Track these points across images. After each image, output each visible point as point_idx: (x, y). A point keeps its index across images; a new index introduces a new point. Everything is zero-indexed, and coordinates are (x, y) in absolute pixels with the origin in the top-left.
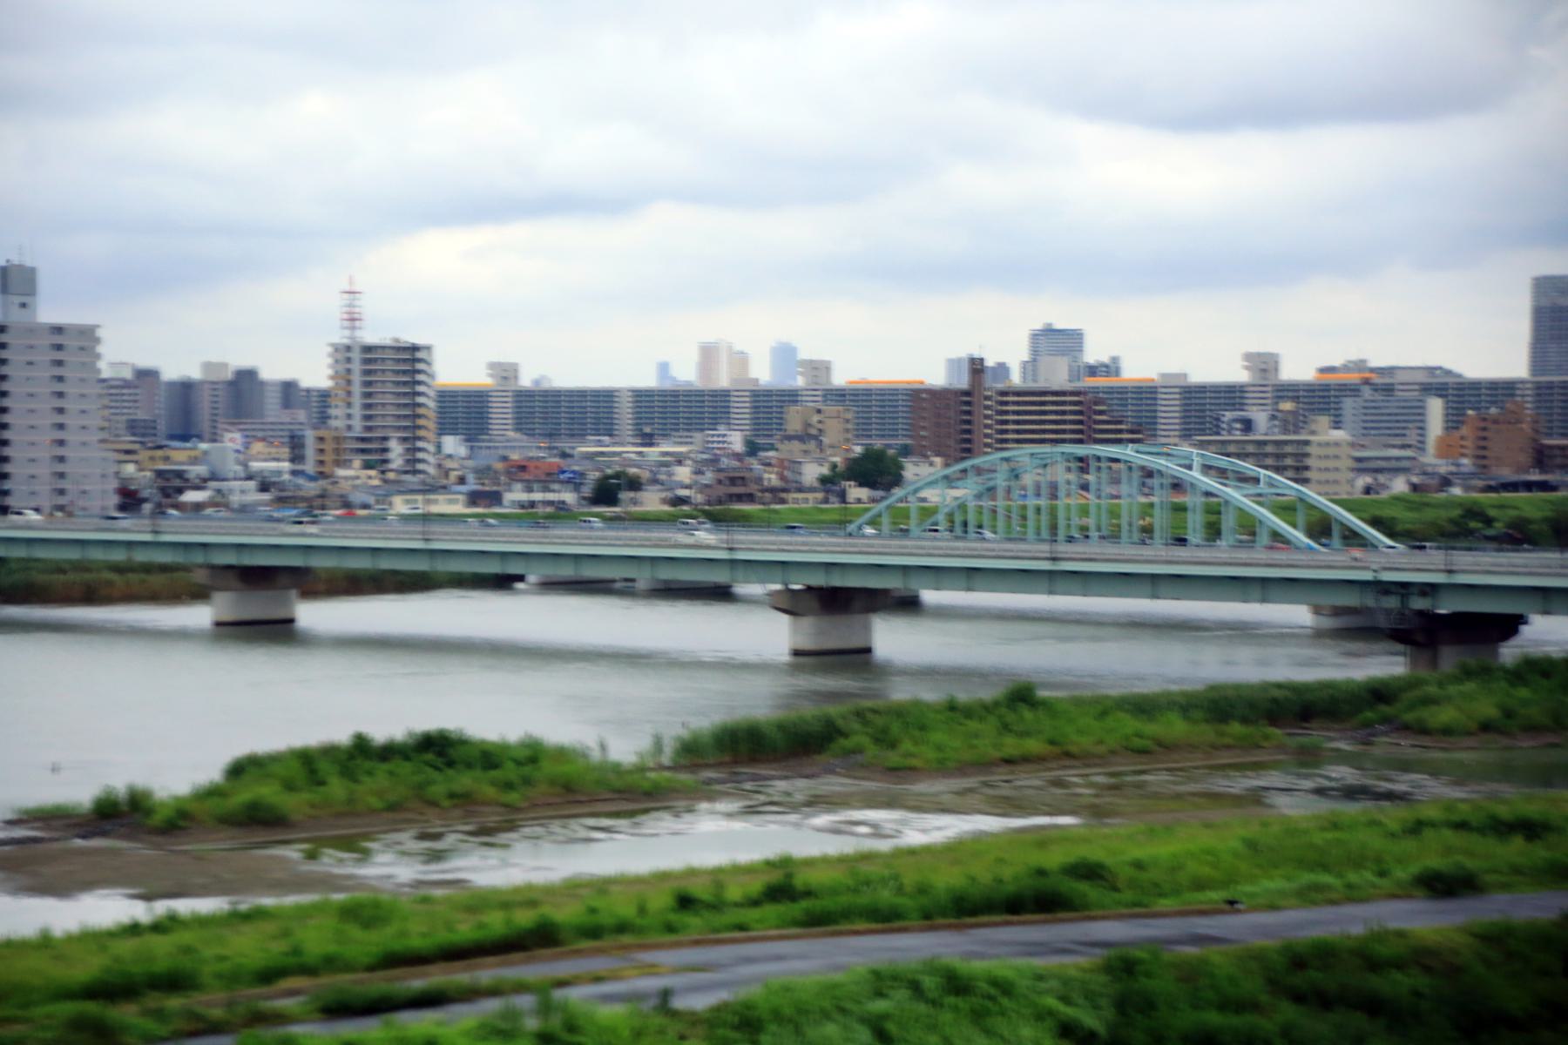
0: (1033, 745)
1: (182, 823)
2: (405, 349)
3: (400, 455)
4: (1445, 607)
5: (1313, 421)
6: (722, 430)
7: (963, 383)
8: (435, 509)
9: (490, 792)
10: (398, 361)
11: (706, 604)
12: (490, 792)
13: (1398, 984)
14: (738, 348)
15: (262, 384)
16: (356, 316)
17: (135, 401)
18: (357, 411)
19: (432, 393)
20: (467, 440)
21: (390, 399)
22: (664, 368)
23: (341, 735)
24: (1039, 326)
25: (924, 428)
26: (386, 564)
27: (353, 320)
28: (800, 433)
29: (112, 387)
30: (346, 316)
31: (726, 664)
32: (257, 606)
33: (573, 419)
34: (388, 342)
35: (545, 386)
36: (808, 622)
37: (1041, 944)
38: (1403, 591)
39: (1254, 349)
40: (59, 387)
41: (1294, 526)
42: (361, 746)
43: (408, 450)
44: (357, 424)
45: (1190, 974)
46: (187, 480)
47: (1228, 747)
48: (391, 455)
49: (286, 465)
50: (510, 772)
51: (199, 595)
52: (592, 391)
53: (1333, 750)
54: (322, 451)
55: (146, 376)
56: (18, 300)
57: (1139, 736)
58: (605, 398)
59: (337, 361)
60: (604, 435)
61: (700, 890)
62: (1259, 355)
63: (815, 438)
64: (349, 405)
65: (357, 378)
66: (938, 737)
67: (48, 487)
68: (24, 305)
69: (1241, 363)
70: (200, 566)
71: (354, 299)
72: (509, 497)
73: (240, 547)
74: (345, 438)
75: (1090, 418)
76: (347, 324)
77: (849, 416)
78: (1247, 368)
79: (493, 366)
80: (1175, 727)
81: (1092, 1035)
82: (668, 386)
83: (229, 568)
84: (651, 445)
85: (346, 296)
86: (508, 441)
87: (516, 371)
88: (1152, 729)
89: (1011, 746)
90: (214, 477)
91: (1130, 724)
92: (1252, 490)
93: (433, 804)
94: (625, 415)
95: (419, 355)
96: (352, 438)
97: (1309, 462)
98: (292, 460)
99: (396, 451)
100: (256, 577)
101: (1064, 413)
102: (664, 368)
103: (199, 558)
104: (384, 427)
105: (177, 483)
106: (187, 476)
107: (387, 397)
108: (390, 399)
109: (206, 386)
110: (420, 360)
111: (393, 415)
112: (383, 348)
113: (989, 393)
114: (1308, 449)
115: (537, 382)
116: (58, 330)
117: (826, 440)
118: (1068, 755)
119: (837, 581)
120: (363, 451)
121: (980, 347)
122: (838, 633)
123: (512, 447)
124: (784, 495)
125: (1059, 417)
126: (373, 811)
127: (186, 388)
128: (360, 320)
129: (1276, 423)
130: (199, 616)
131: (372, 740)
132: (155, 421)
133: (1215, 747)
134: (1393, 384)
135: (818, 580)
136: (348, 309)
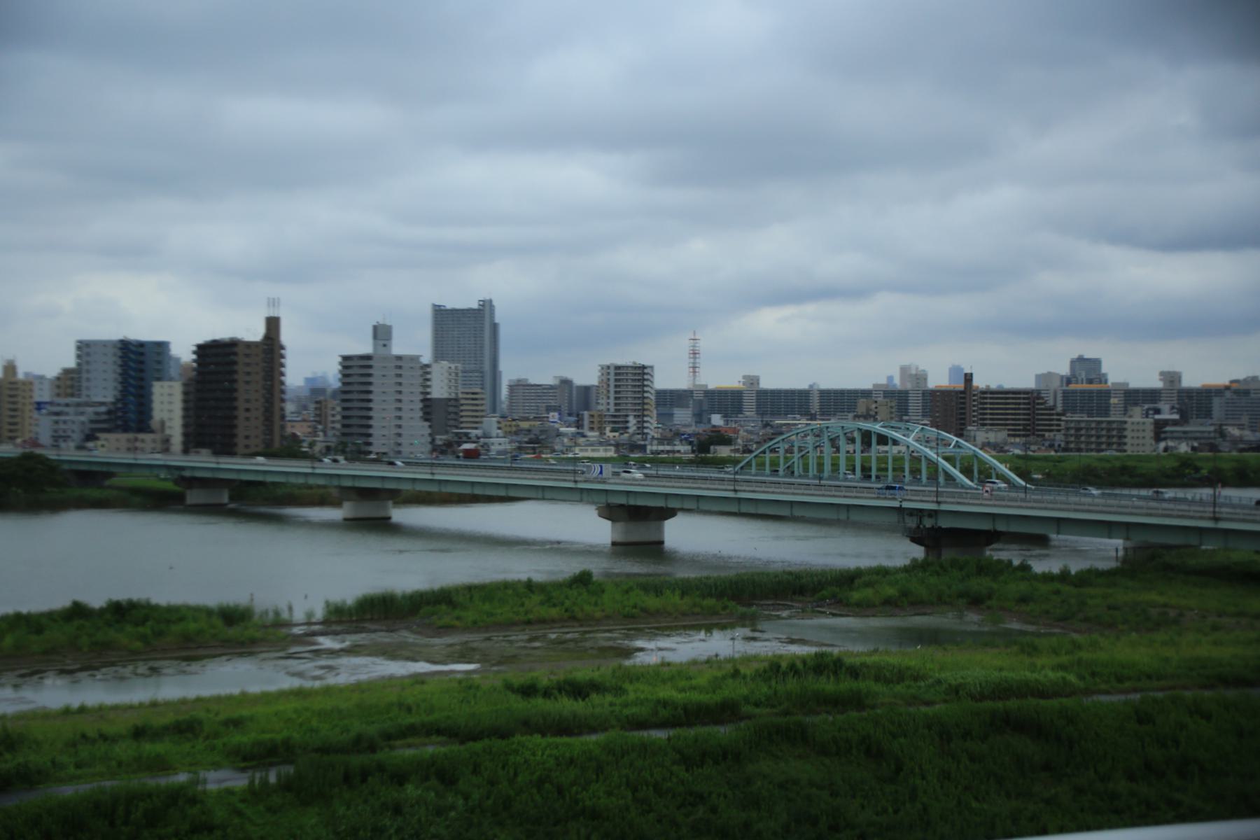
4: (945, 523)
5: (1132, 410)
7: (960, 386)
10: (635, 374)
11: (333, 520)
16: (697, 352)
17: (555, 396)
18: (612, 401)
19: (653, 392)
20: (724, 417)
21: (630, 395)
23: (60, 602)
24: (1075, 356)
25: (938, 412)
27: (695, 354)
28: (865, 414)
30: (691, 352)
31: (590, 552)
32: (368, 510)
33: (788, 405)
34: (631, 364)
36: (620, 526)
38: (920, 514)
39: (1166, 369)
40: (399, 388)
41: (955, 467)
42: (78, 611)
43: (639, 422)
44: (612, 408)
46: (470, 438)
51: (336, 504)
52: (848, 391)
54: (592, 422)
55: (566, 383)
56: (382, 342)
59: (603, 374)
60: (798, 414)
62: (1169, 373)
63: (874, 417)
64: (608, 398)
65: (612, 383)
67: (392, 442)
68: (385, 345)
69: (1157, 377)
71: (696, 343)
73: (354, 477)
74: (605, 415)
76: (692, 356)
77: (893, 404)
78: (1161, 380)
85: (692, 341)
86: (747, 417)
87: (758, 380)
94: (815, 406)
95: (646, 371)
96: (610, 415)
97: (1126, 433)
98: (578, 427)
99: (632, 421)
101: (1019, 404)
103: (335, 482)
104: (627, 409)
106: (470, 435)
108: (630, 395)
109: (594, 388)
110: (647, 374)
111: (631, 403)
112: (627, 367)
113: (976, 393)
114: (1126, 426)
116: (399, 358)
118: (573, 618)
119: (640, 502)
122: (641, 533)
123: (749, 421)
125: (1017, 406)
128: (698, 353)
129: (1175, 410)
132: (560, 407)
133: (684, 614)
134: (1249, 390)
135: (622, 500)
136: (691, 348)
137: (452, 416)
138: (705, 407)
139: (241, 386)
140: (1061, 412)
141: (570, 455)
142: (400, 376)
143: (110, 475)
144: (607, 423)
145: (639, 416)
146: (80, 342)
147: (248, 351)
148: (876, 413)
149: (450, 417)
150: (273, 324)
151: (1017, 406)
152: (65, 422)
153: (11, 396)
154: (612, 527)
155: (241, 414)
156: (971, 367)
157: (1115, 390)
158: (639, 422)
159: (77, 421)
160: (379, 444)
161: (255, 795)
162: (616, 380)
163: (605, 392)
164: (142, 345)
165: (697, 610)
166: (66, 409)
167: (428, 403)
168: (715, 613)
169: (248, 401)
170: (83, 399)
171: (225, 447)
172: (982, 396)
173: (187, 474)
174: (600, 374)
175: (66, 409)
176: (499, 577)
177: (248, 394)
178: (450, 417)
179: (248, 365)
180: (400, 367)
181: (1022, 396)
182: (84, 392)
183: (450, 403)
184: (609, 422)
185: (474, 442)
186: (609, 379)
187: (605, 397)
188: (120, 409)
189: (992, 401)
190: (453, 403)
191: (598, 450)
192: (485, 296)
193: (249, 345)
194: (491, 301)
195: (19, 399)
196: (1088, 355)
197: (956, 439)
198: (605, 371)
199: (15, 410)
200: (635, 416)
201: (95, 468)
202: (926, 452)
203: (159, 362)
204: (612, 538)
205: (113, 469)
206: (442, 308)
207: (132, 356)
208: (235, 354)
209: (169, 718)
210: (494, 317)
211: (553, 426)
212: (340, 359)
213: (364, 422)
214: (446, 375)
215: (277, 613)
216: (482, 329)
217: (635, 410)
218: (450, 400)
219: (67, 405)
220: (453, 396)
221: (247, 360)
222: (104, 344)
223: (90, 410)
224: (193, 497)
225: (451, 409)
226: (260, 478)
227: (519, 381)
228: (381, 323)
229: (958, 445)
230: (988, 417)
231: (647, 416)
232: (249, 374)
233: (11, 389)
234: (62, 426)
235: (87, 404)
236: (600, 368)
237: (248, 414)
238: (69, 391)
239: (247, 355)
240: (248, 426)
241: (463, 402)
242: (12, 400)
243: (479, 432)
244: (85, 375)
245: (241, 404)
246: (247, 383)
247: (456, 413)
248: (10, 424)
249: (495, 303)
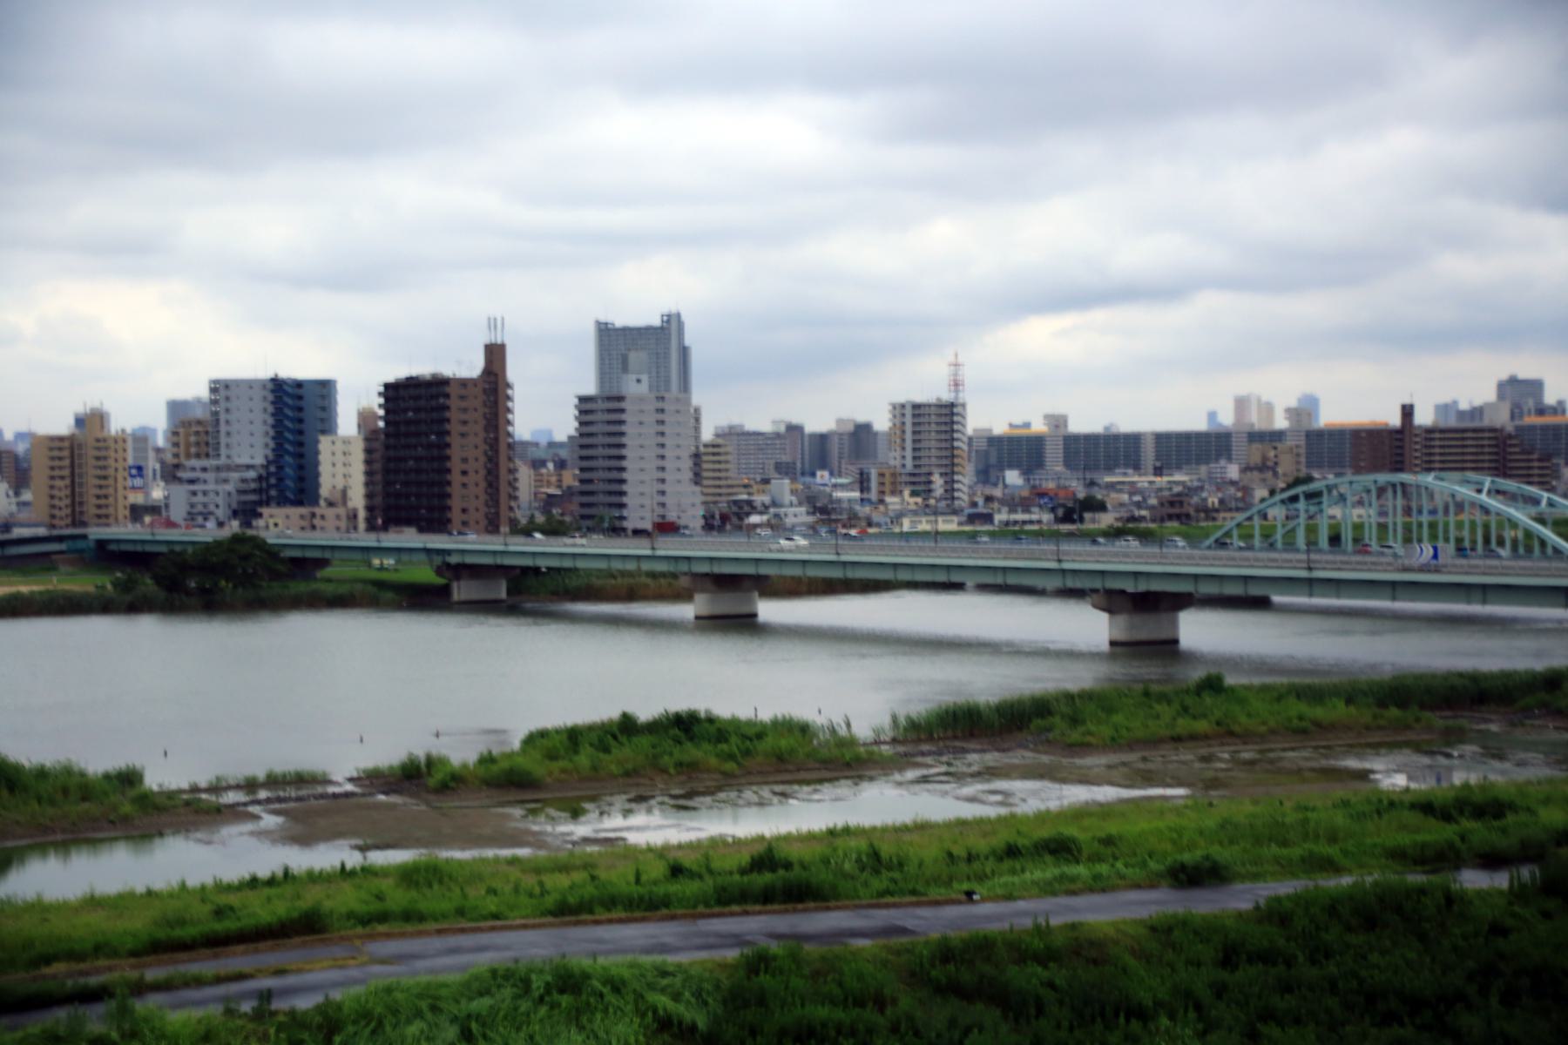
0: (1202, 726)
1: (452, 784)
2: (945, 406)
3: (941, 486)
6: (1223, 462)
7: (1395, 420)
8: (512, 548)
9: (713, 761)
12: (713, 761)
13: (1028, 977)
14: (1265, 398)
15: (876, 434)
18: (909, 453)
22: (1212, 416)
24: (1504, 376)
26: (812, 572)
29: (769, 439)
32: (728, 604)
35: (1114, 430)
36: (1122, 620)
37: (735, 936)
42: (627, 725)
44: (909, 463)
45: (825, 970)
47: (1380, 728)
48: (933, 486)
49: (856, 495)
50: (734, 744)
51: (683, 596)
53: (1479, 731)
55: (794, 430)
56: (634, 377)
57: (1301, 718)
58: (1134, 440)
59: (895, 416)
61: (688, 861)
65: (909, 428)
66: (1118, 718)
70: (686, 574)
72: (998, 518)
73: (711, 560)
74: (900, 474)
75: (1504, 450)
78: (1045, 424)
79: (1047, 417)
80: (1338, 710)
81: (693, 1028)
82: (1214, 429)
83: (706, 575)
84: (1161, 475)
88: (1319, 712)
89: (1184, 725)
90: (774, 504)
91: (1296, 708)
92: (1533, 511)
93: (664, 771)
94: (1149, 454)
99: (938, 482)
100: (726, 582)
102: (1212, 416)
103: (684, 567)
105: (746, 509)
106: (755, 504)
107: (931, 441)
112: (930, 406)
115: (1106, 428)
117: (1280, 470)
118: (1231, 734)
119: (1156, 586)
120: (914, 483)
121: (1412, 396)
122: (1148, 628)
124: (1215, 515)
126: (613, 777)
127: (822, 439)
130: (685, 611)
131: (560, 727)
133: (1368, 728)
138: (993, 460)
139: (454, 440)
141: (897, 530)
142: (662, 422)
143: (322, 563)
144: (903, 485)
145: (946, 474)
146: (215, 382)
147: (463, 392)
148: (1276, 464)
150: (495, 354)
151: (1479, 450)
152: (205, 493)
153: (98, 458)
154: (1110, 620)
155: (456, 478)
156: (1412, 396)
157: (1237, 433)
158: (946, 482)
159: (221, 492)
160: (639, 513)
161: (1518, 894)
162: (914, 424)
163: (898, 441)
164: (299, 384)
165: (1382, 722)
166: (202, 475)
168: (1408, 727)
169: (465, 460)
170: (223, 461)
171: (436, 522)
172: (1428, 436)
173: (454, 560)
174: (890, 416)
175: (202, 475)
176: (599, 710)
177: (465, 450)
179: (465, 410)
180: (662, 411)
181: (1487, 435)
182: (223, 451)
184: (906, 483)
185: (761, 513)
186: (903, 423)
187: (898, 449)
189: (1442, 443)
192: (669, 306)
193: (464, 383)
194: (678, 315)
195: (111, 462)
196: (1523, 374)
197: (1546, 495)
198: (897, 412)
199: (105, 478)
200: (941, 474)
201: (309, 554)
202: (1509, 513)
203: (324, 409)
204: (1110, 635)
205: (327, 555)
206: (610, 326)
207: (290, 401)
208: (447, 396)
209: (139, 924)
210: (683, 339)
211: (824, 491)
212: (576, 401)
213: (615, 487)
215: (833, 731)
216: (667, 355)
217: (941, 466)
219: (204, 470)
222: (250, 384)
223: (235, 476)
224: (461, 591)
226: (567, 564)
227: (731, 427)
229: (1551, 504)
230: (1437, 458)
231: (958, 473)
233: (98, 449)
234: (200, 498)
235: (229, 468)
236: (890, 408)
237: (465, 479)
238: (204, 449)
239: (462, 398)
240: (465, 491)
242: (101, 463)
243: (766, 499)
244: (223, 428)
245: (455, 465)
246: (463, 435)
248: (98, 497)
249: (684, 318)
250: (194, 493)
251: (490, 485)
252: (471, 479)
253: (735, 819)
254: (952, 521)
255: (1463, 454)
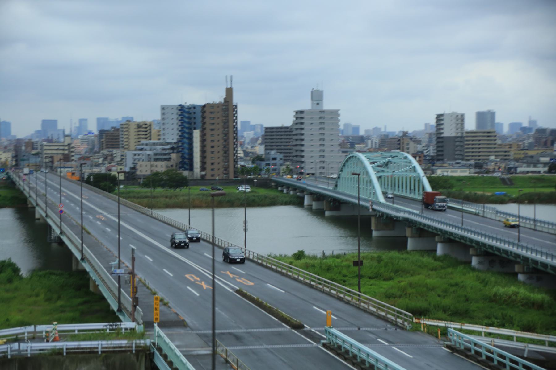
137: (459, 148)
140: (98, 151)
149: (457, 149)
167: (440, 140)
178: (457, 149)
183: (456, 140)
188: (181, 146)
190: (459, 139)
191: (456, 172)
212: (294, 114)
214: (454, 121)
218: (457, 137)
219: (147, 145)
220: (459, 135)
221: (212, 116)
225: (457, 143)
228: (315, 89)
232: (213, 124)
237: (212, 150)
241: (466, 139)
246: (212, 130)
247: (461, 146)
250: (135, 155)
251: (225, 152)
252: (216, 149)
253: (429, 321)
254: (466, 171)
255: (473, 144)
